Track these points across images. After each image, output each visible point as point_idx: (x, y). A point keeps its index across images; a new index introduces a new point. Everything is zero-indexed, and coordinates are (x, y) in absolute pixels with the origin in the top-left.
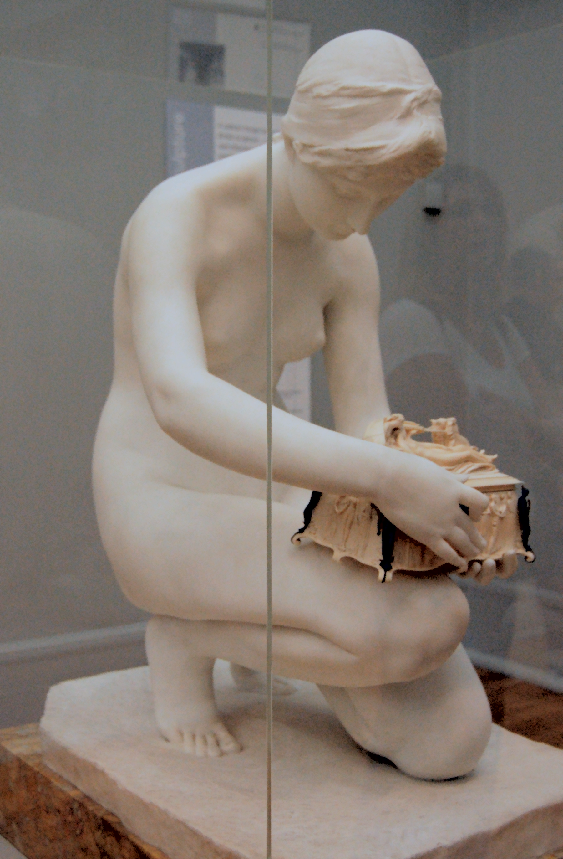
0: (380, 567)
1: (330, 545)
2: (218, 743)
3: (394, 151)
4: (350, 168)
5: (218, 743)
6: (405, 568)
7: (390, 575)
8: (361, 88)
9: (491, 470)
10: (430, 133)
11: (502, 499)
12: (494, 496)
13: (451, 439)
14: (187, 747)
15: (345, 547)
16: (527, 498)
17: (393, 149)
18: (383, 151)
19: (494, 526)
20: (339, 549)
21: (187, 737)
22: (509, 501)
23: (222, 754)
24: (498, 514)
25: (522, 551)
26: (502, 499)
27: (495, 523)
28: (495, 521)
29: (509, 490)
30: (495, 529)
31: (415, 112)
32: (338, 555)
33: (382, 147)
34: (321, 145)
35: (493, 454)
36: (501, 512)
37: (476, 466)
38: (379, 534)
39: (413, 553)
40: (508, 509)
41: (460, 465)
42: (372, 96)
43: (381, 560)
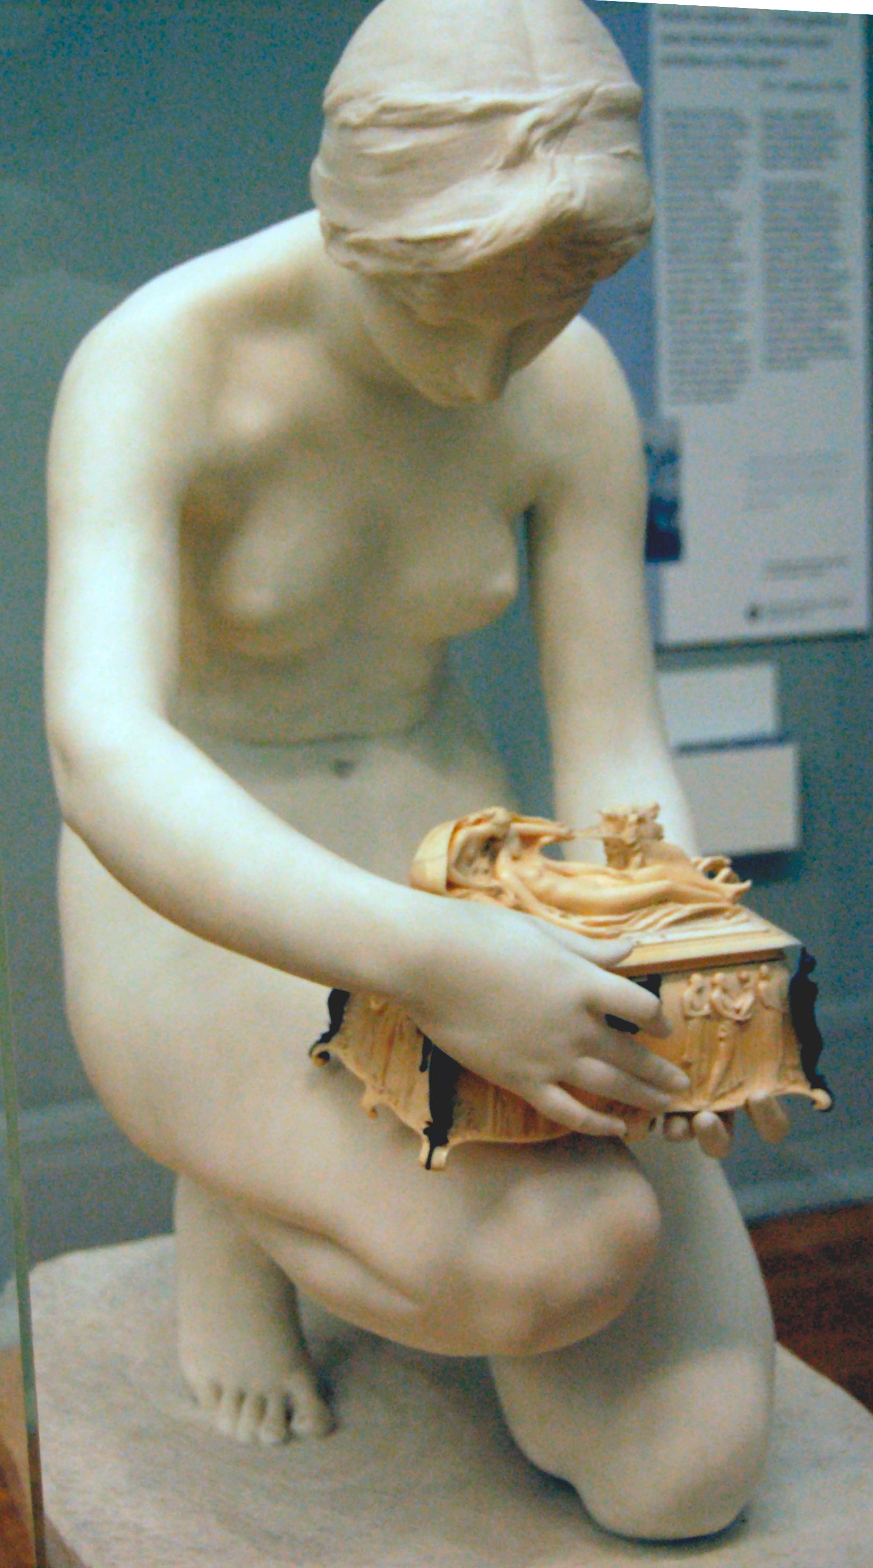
0: (426, 1131)
1: (363, 1076)
2: (288, 1416)
3: (489, 243)
4: (416, 278)
5: (288, 1416)
6: (486, 1136)
7: (441, 1155)
8: (421, 107)
9: (728, 918)
10: (571, 195)
11: (743, 981)
12: (719, 976)
13: (636, 853)
14: (224, 1424)
15: (383, 1084)
16: (812, 977)
17: (486, 238)
18: (467, 243)
19: (721, 1039)
20: (374, 1087)
21: (227, 1401)
22: (762, 985)
23: (289, 1437)
24: (731, 1014)
25: (801, 1088)
26: (743, 981)
27: (723, 1034)
28: (723, 1030)
29: (762, 962)
30: (722, 1045)
31: (539, 152)
32: (370, 1098)
33: (465, 234)
34: (355, 230)
35: (743, 880)
36: (738, 1011)
37: (687, 909)
38: (422, 1069)
39: (504, 1106)
40: (759, 1001)
41: (645, 911)
42: (450, 123)
43: (428, 1123)
